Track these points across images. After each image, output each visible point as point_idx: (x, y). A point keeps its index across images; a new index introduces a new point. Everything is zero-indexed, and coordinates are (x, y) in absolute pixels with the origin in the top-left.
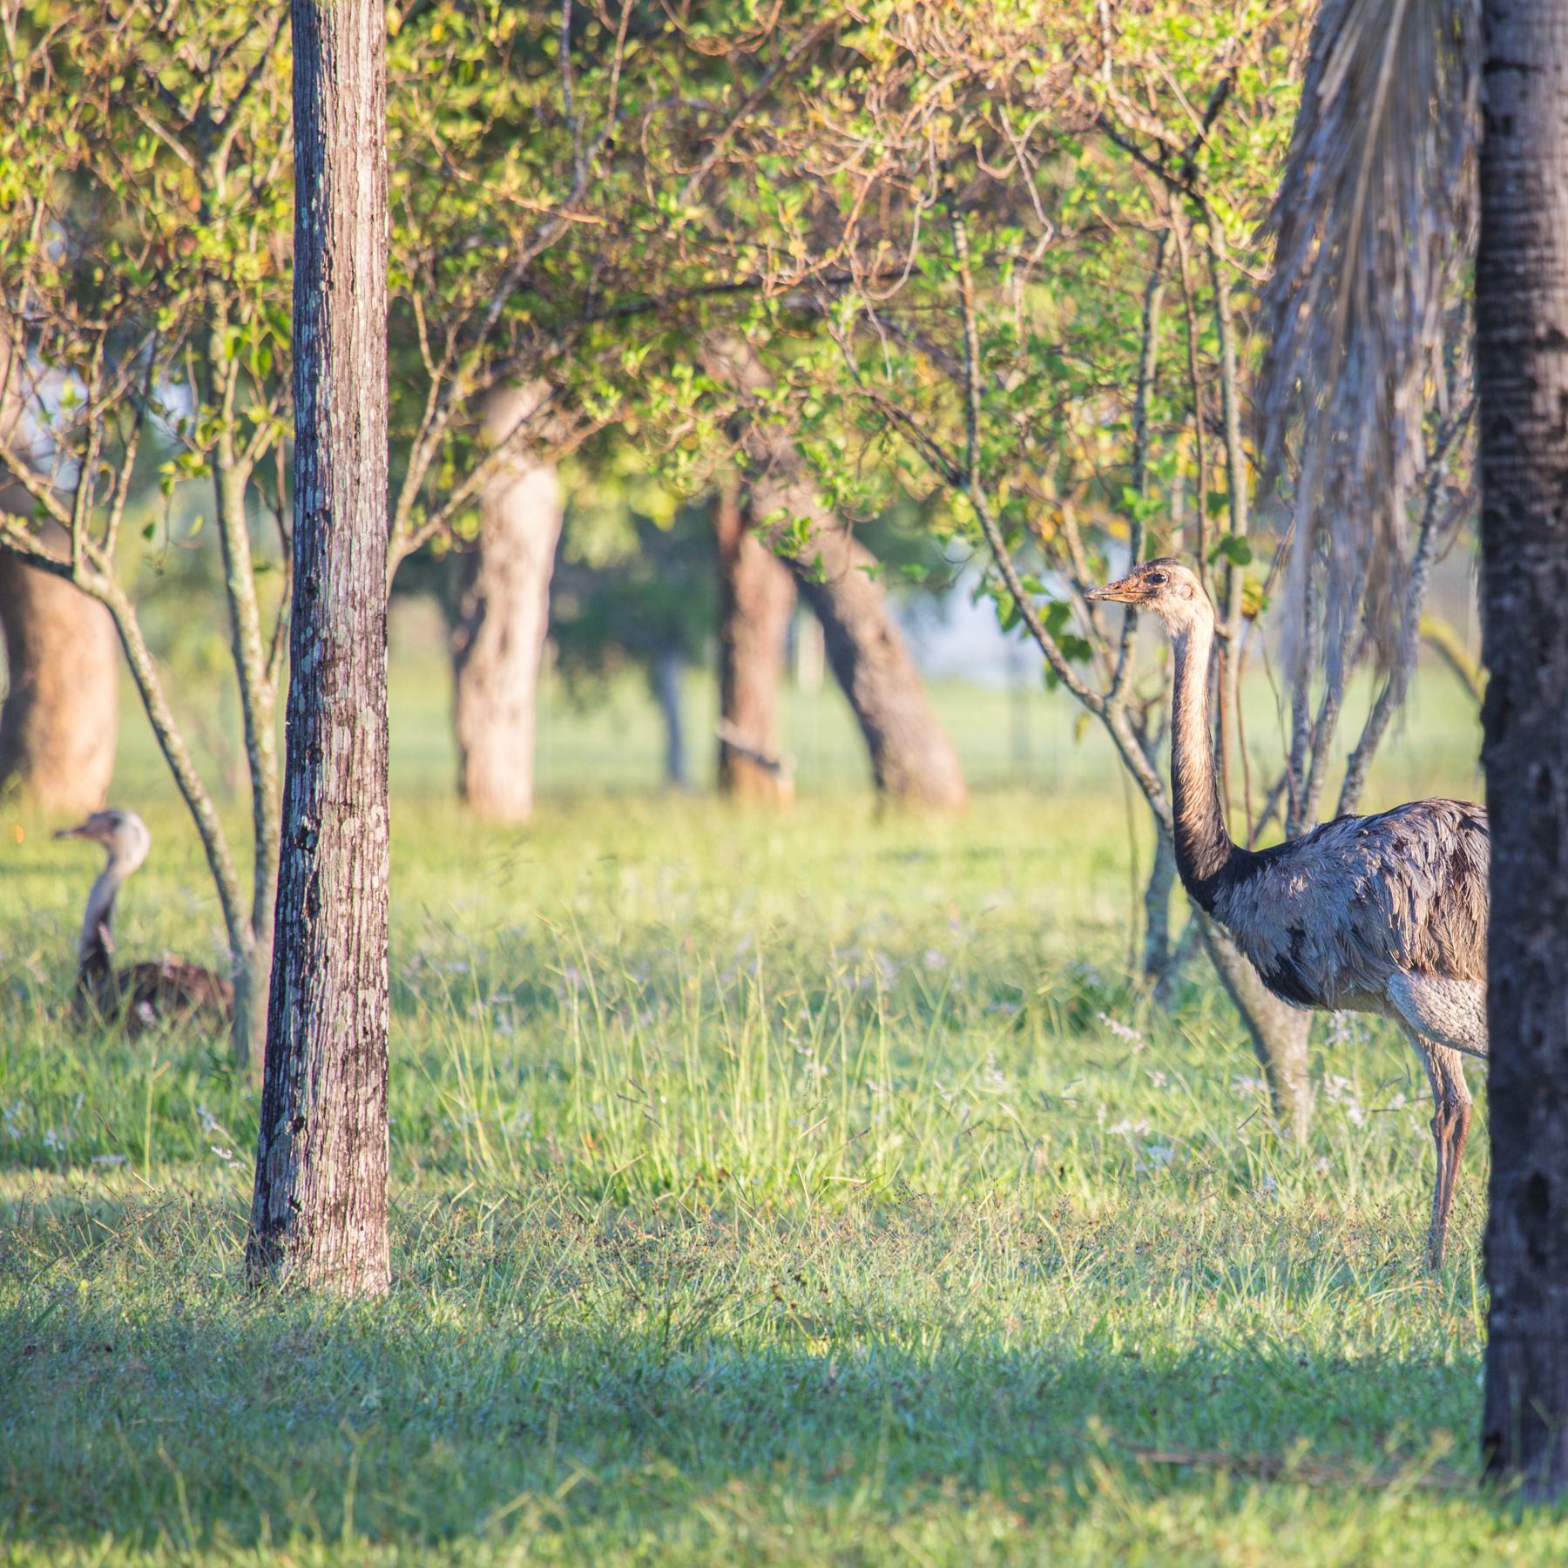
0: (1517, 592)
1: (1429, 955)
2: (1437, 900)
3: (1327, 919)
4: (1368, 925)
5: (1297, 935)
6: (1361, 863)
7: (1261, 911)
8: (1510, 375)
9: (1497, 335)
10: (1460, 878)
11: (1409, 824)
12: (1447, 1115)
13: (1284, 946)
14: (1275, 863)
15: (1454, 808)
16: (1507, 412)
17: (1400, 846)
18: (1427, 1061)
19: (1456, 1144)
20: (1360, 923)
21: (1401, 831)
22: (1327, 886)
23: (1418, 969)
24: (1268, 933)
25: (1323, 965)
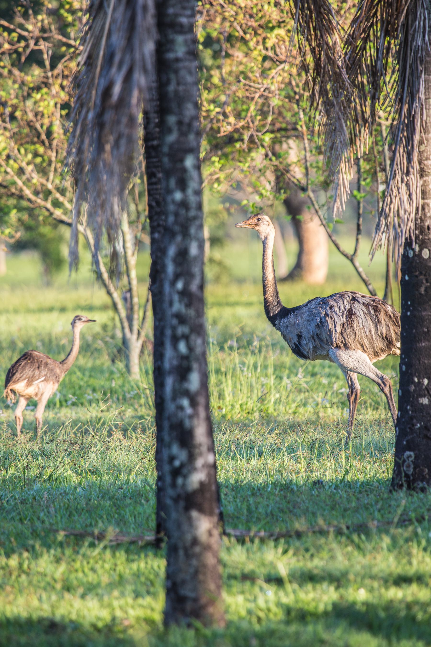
0: (159, 232)
1: (342, 342)
2: (343, 324)
3: (309, 332)
4: (321, 333)
5: (300, 337)
6: (319, 313)
7: (289, 328)
8: (155, 157)
9: (150, 143)
10: (350, 318)
11: (335, 300)
12: (352, 392)
13: (295, 340)
14: (294, 312)
15: (350, 294)
16: (154, 170)
17: (331, 307)
18: (346, 376)
19: (355, 402)
20: (319, 332)
21: (332, 303)
22: (308, 321)
23: (338, 347)
24: (292, 336)
25: (308, 346)
